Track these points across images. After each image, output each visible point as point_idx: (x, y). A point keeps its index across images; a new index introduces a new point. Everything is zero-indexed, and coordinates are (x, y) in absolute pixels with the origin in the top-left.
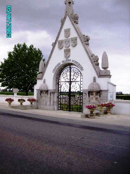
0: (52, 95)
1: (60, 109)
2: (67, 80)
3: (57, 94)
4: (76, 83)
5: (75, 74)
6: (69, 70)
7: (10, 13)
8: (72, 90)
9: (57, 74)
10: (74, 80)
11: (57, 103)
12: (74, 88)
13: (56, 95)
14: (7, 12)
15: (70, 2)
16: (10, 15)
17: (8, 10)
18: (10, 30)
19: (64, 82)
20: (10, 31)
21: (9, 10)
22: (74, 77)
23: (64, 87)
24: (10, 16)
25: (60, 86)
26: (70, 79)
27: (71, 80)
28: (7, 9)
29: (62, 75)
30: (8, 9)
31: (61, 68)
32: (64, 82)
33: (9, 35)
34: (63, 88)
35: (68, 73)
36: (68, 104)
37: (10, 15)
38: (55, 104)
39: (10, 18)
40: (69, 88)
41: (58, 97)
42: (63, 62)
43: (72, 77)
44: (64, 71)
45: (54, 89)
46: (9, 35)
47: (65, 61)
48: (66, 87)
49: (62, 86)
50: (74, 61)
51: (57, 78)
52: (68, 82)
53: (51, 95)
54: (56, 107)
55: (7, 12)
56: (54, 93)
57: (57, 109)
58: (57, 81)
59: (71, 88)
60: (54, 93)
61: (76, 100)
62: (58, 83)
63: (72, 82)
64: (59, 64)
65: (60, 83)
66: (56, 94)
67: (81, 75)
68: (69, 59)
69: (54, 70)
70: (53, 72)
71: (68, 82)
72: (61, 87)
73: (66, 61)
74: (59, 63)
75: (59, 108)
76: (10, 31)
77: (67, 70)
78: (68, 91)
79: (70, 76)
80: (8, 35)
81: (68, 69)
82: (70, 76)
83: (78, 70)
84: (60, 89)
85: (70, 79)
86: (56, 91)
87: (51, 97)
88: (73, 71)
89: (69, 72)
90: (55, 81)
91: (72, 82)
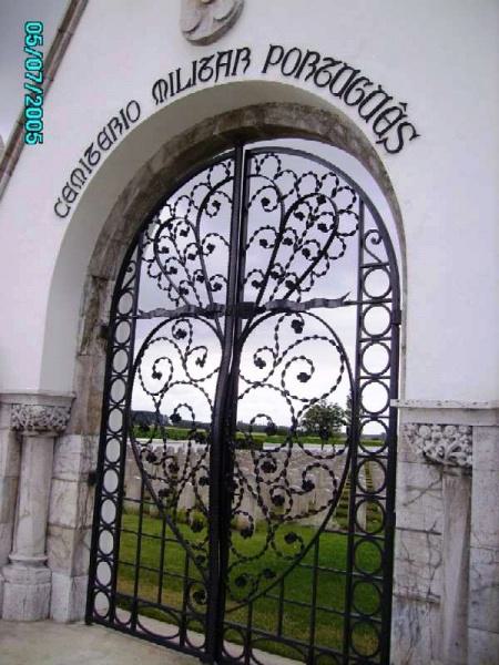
0: (35, 451)
1: (110, 622)
2: (199, 296)
3: (87, 445)
4: (298, 326)
5: (292, 222)
6: (228, 188)
7: (37, 48)
8: (245, 413)
9: (104, 234)
10: (283, 290)
11: (79, 542)
12: (275, 380)
13: (75, 452)
14: (28, 47)
15: (293, 326)
16: (38, 57)
17: (32, 39)
18: (38, 113)
19: (172, 316)
20: (40, 119)
21: (35, 37)
22: (285, 252)
23: (163, 368)
24: (38, 60)
25: (120, 361)
26: (237, 278)
27: (250, 294)
28: (28, 34)
29: (149, 253)
30: (32, 35)
31: (148, 166)
32: (172, 316)
33: (35, 135)
34: (157, 385)
35: (218, 225)
36: (195, 574)
37: (38, 57)
38: (62, 549)
39: (38, 68)
40: (211, 386)
41: (95, 479)
42: (161, 87)
43: (256, 259)
44: (178, 207)
45: (64, 381)
46: (35, 135)
47: (186, 77)
48: (179, 375)
49: (146, 367)
50: (284, 59)
51: (98, 281)
52: (211, 312)
53: (27, 450)
54: (65, 591)
55: (28, 47)
56: (54, 434)
57: (83, 613)
58: (96, 304)
59: (242, 386)
60: (61, 434)
61: (291, 538)
62: (108, 333)
63: (253, 310)
64: (122, 120)
65: (122, 332)
66: (74, 445)
67: (370, 224)
68: (232, 42)
69: (68, 193)
70: (62, 209)
71: (211, 312)
72: (133, 367)
73: (196, 75)
74: (124, 114)
75: (102, 603)
76: (40, 119)
77: (203, 192)
78: (204, 416)
79: (238, 250)
80: (33, 132)
81: (218, 173)
82: (238, 250)
83: (335, 171)
84: (118, 391)
85: (237, 278)
86: (82, 410)
87: (25, 474)
88: (271, 195)
89: (226, 208)
90: (75, 303)
91: (253, 310)
